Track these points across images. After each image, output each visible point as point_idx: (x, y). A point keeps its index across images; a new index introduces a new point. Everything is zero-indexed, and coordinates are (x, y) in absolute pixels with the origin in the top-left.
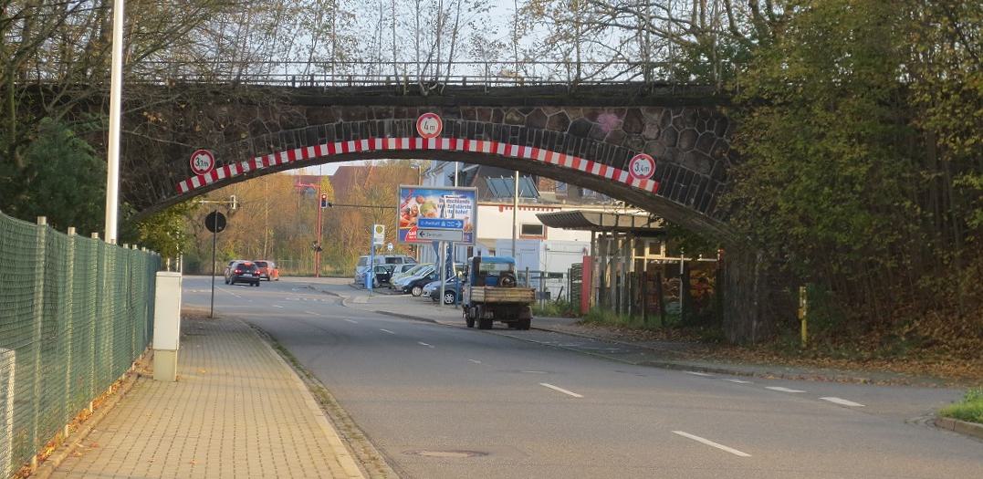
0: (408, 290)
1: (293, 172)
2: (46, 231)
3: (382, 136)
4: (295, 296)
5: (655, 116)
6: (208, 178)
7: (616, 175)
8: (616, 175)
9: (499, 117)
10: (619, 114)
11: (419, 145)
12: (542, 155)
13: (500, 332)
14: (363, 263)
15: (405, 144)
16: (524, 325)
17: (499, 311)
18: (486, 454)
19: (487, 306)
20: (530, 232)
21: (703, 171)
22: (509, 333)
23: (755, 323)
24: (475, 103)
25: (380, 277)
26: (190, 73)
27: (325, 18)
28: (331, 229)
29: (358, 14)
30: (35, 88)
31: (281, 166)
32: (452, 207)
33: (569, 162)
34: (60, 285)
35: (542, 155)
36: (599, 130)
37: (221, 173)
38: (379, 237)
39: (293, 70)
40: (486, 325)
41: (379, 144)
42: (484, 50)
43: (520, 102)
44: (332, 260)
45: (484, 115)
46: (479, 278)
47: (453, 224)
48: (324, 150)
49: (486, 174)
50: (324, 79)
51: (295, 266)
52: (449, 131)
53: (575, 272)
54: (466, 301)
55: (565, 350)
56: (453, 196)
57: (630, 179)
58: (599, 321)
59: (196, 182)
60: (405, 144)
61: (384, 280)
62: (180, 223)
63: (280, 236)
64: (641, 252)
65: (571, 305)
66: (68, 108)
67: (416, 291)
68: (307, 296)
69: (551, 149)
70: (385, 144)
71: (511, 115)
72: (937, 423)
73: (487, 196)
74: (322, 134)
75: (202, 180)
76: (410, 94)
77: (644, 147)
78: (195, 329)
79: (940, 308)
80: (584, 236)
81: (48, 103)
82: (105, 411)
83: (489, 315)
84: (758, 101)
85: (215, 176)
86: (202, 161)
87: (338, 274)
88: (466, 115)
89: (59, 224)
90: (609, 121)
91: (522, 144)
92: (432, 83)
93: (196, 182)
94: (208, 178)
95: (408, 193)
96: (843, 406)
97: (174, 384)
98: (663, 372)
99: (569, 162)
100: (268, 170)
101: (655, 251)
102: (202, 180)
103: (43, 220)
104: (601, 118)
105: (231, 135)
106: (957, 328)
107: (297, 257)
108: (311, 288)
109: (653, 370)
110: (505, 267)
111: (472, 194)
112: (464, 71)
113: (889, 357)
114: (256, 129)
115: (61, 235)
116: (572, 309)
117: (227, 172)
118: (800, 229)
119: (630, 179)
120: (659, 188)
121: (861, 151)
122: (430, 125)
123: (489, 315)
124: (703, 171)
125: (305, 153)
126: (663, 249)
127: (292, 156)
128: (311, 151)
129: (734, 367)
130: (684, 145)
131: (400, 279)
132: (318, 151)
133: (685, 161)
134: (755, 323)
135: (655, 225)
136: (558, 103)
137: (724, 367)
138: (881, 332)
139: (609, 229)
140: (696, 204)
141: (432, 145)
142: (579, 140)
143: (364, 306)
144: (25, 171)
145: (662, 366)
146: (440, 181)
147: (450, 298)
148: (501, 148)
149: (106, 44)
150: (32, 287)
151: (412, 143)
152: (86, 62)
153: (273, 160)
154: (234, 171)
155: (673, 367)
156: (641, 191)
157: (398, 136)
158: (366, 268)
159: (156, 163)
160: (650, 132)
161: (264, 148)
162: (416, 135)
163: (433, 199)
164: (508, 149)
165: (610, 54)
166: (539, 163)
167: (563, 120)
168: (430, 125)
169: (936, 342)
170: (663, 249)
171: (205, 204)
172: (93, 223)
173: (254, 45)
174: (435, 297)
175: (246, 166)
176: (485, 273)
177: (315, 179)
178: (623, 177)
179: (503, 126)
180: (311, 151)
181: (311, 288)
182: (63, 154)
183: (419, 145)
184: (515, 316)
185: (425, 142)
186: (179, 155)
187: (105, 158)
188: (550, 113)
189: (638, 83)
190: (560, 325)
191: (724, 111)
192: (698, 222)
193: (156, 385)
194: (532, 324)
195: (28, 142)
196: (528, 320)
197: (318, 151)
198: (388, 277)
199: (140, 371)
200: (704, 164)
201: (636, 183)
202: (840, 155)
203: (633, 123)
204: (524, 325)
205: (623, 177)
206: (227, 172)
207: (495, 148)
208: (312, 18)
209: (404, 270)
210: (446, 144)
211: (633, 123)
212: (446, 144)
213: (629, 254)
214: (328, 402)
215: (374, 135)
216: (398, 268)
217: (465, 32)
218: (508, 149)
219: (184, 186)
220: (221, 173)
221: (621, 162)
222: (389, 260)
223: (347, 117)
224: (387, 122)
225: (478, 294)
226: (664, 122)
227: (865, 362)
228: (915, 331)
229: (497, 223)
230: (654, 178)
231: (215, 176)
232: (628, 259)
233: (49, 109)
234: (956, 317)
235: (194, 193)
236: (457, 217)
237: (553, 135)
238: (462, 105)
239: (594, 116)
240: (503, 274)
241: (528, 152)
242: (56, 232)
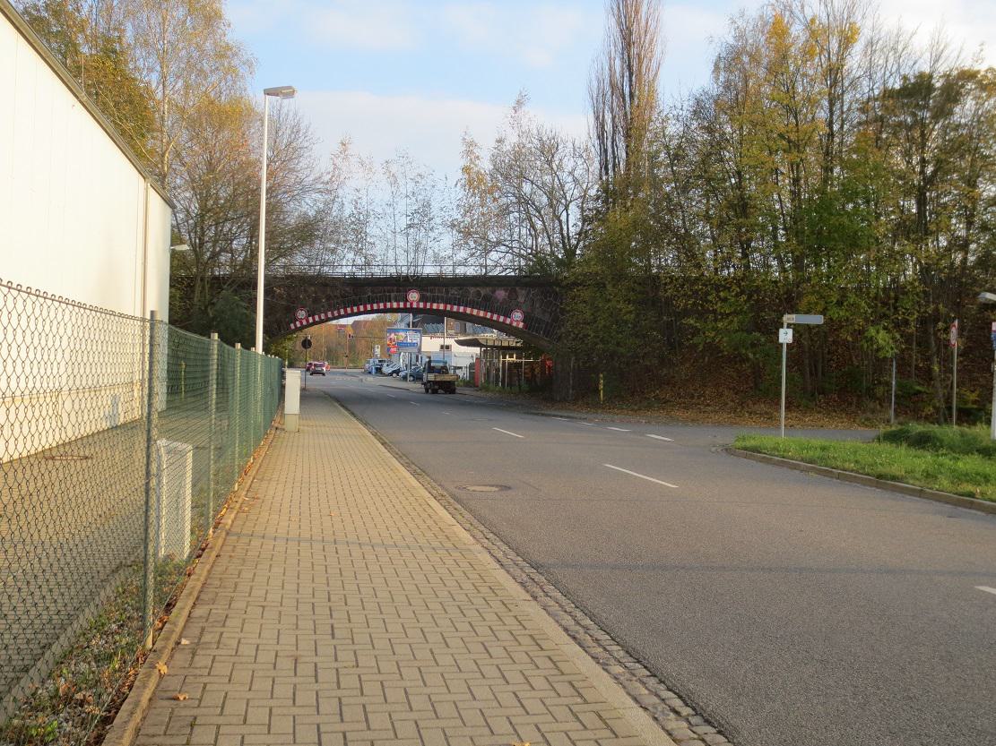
0: (391, 374)
1: (334, 322)
2: (218, 345)
3: (390, 301)
4: (340, 378)
5: (524, 292)
6: (304, 323)
7: (505, 320)
8: (505, 320)
9: (447, 292)
10: (506, 291)
11: (408, 306)
12: (469, 311)
13: (442, 396)
14: (368, 362)
15: (402, 305)
16: (453, 391)
17: (439, 385)
18: (510, 488)
19: (435, 383)
20: (455, 350)
21: (547, 318)
22: (446, 396)
23: (571, 391)
24: (436, 285)
25: (377, 369)
26: (295, 271)
27: (360, 245)
28: (352, 348)
29: (376, 243)
30: (216, 278)
31: (328, 320)
32: (412, 337)
33: (482, 314)
34: (230, 386)
35: (469, 311)
36: (496, 298)
37: (311, 320)
38: (378, 351)
39: (345, 270)
40: (435, 392)
41: (388, 305)
42: (438, 260)
43: (458, 285)
44: (352, 361)
45: (439, 291)
46: (431, 369)
47: (413, 345)
48: (362, 308)
49: (428, 319)
50: (360, 274)
51: (337, 364)
52: (423, 299)
53: (471, 366)
54: (425, 381)
55: (478, 405)
56: (411, 332)
57: (511, 322)
58: (487, 389)
59: (298, 324)
60: (402, 305)
61: (379, 370)
62: (289, 344)
63: (329, 351)
64: (504, 357)
65: (469, 382)
66: (235, 287)
67: (394, 375)
68: (345, 378)
69: (473, 308)
70: (391, 305)
71: (454, 291)
72: (728, 450)
73: (425, 333)
74: (360, 300)
75: (301, 323)
76: (404, 281)
77: (518, 307)
78: (306, 396)
79: (668, 384)
80: (477, 350)
81: (224, 284)
82: (261, 458)
83: (436, 387)
84: (575, 284)
85: (308, 321)
86: (301, 314)
87: (355, 368)
88: (431, 291)
89: (228, 340)
90: (501, 294)
91: (459, 305)
92: (414, 276)
93: (298, 324)
94: (304, 323)
95: (391, 331)
96: (665, 441)
97: (297, 434)
98: (536, 417)
99: (482, 314)
100: (322, 321)
101: (511, 356)
102: (301, 323)
103: (216, 336)
104: (497, 292)
105: (316, 300)
106: (679, 394)
107: (337, 360)
108: (345, 374)
109: (531, 416)
110: (441, 365)
111: (419, 331)
112: (430, 270)
113: (649, 407)
114: (329, 298)
115: (231, 348)
116: (471, 383)
117: (314, 319)
118: (600, 346)
119: (511, 322)
120: (526, 326)
121: (631, 307)
122: (414, 296)
123: (436, 387)
124: (547, 318)
125: (352, 310)
126: (515, 356)
127: (346, 311)
128: (355, 309)
129: (556, 413)
130: (537, 306)
131: (386, 370)
132: (358, 309)
133: (538, 313)
134: (571, 391)
135: (519, 345)
136: (476, 285)
137: (571, 415)
138: (639, 395)
139: (490, 346)
140: (544, 333)
141: (415, 306)
142: (486, 304)
143: (373, 382)
144: (213, 318)
145: (537, 414)
146: (403, 326)
147: (412, 378)
148: (449, 308)
149: (254, 256)
150: (207, 403)
151: (405, 305)
152: (243, 266)
153: (369, 308)
154: (317, 318)
155: (543, 415)
156: (517, 328)
157: (398, 301)
158: (371, 364)
159: (278, 315)
160: (521, 299)
161: (331, 307)
162: (407, 301)
163: (402, 334)
164: (452, 308)
165: (500, 262)
166: (468, 314)
167: (479, 294)
168: (414, 296)
169: (668, 401)
170: (515, 356)
171: (301, 336)
172: (249, 343)
173: (329, 257)
174: (405, 378)
175: (349, 310)
176: (434, 367)
177: (344, 326)
178: (508, 321)
179: (438, 298)
180: (355, 309)
181: (345, 374)
182: (232, 310)
183: (408, 306)
184: (448, 387)
185: (411, 304)
186: (290, 312)
187: (256, 313)
188: (472, 290)
189: (512, 276)
190: (468, 391)
191: (558, 289)
192: (545, 344)
193: (287, 434)
194: (457, 391)
195: (213, 304)
196: (455, 390)
197: (358, 309)
198: (380, 369)
199: (276, 425)
200: (547, 315)
201: (515, 324)
202: (621, 310)
203: (513, 294)
204: (453, 391)
205: (508, 321)
206: (314, 319)
207: (446, 307)
208: (353, 245)
209: (388, 365)
210: (421, 305)
211: (513, 294)
212: (421, 305)
213: (499, 358)
214: (386, 443)
215: (386, 301)
216: (385, 365)
217: (430, 252)
218: (452, 308)
219: (292, 326)
220: (311, 320)
221: (507, 315)
222: (380, 361)
223: (373, 292)
224: (392, 295)
225: (431, 377)
226: (528, 294)
227: (636, 411)
228: (657, 395)
229: (430, 345)
230: (523, 322)
231: (308, 321)
232: (499, 361)
233: (225, 286)
234: (677, 388)
235: (297, 329)
236: (415, 341)
237: (474, 301)
238: (432, 286)
239: (494, 292)
240: (443, 368)
241: (461, 309)
242: (225, 345)
